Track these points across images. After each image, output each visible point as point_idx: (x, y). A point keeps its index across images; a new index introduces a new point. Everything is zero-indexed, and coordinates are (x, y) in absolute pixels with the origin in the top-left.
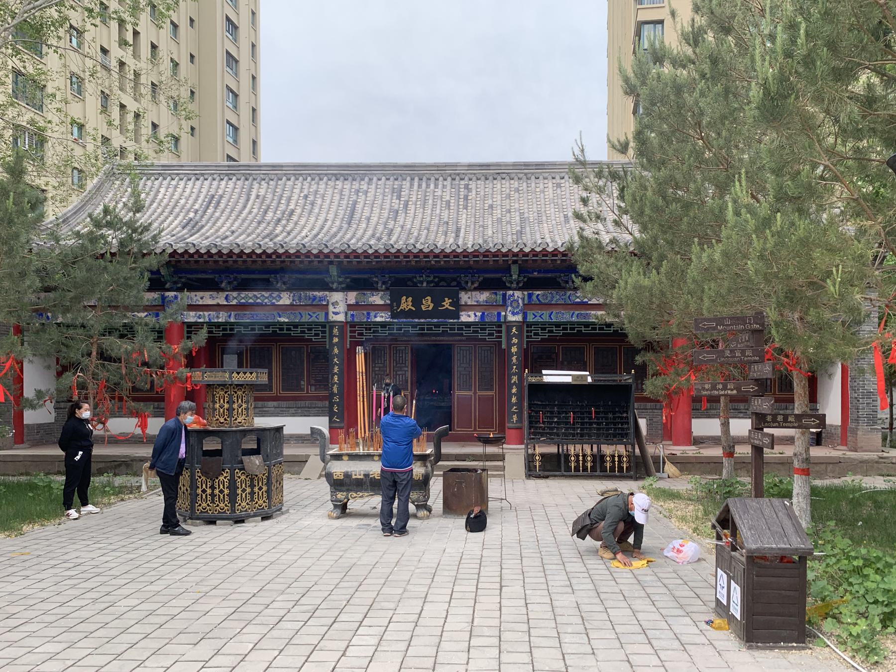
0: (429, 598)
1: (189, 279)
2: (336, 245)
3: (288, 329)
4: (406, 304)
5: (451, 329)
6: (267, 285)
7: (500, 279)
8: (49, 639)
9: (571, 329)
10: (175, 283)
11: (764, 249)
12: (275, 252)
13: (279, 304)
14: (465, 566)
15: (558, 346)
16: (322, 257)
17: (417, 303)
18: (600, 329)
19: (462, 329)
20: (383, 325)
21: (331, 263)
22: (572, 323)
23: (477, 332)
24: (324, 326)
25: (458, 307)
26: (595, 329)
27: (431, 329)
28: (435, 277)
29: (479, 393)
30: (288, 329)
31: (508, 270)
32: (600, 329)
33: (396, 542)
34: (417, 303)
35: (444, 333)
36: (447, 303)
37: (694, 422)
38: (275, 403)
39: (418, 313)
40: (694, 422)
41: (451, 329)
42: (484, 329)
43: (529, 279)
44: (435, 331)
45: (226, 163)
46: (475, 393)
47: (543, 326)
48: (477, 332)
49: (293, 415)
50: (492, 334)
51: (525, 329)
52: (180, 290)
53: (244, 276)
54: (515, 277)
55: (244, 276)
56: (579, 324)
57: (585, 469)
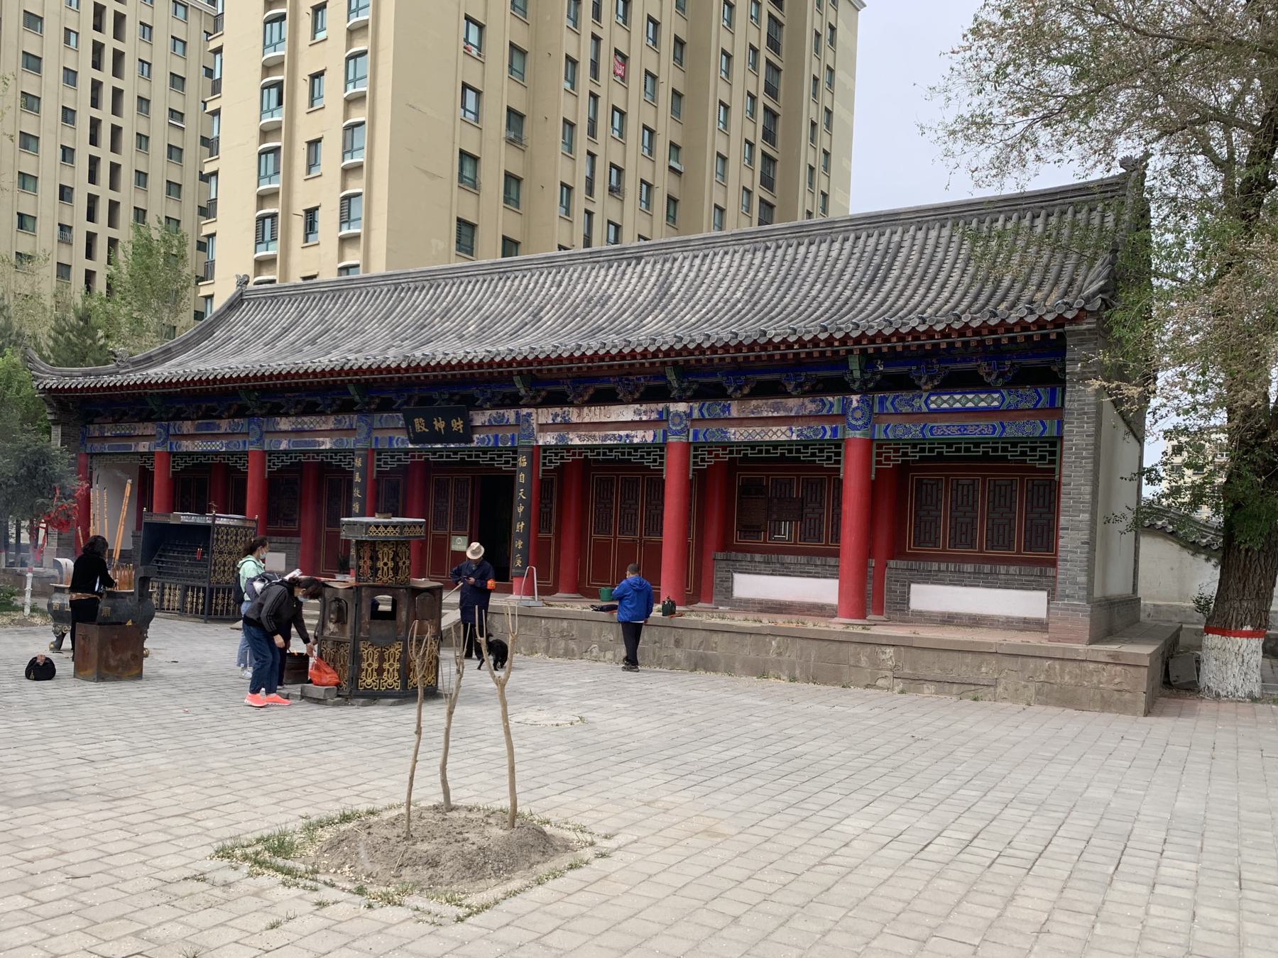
1: (701, 384)
2: (847, 324)
6: (607, 398)
7: (778, 382)
9: (931, 450)
10: (684, 390)
12: (784, 341)
13: (287, 435)
14: (1026, 854)
15: (768, 476)
16: (969, 333)
17: (429, 424)
18: (967, 450)
19: (1005, 449)
20: (286, 452)
21: (850, 352)
25: (470, 429)
29: (620, 537)
30: (477, 456)
31: (843, 363)
32: (967, 450)
38: (283, 539)
41: (470, 456)
43: (549, 392)
45: (636, 244)
47: (898, 445)
49: (1007, 586)
51: (692, 453)
52: (537, 406)
53: (759, 377)
54: (857, 374)
55: (759, 377)
56: (586, 447)
57: (197, 612)
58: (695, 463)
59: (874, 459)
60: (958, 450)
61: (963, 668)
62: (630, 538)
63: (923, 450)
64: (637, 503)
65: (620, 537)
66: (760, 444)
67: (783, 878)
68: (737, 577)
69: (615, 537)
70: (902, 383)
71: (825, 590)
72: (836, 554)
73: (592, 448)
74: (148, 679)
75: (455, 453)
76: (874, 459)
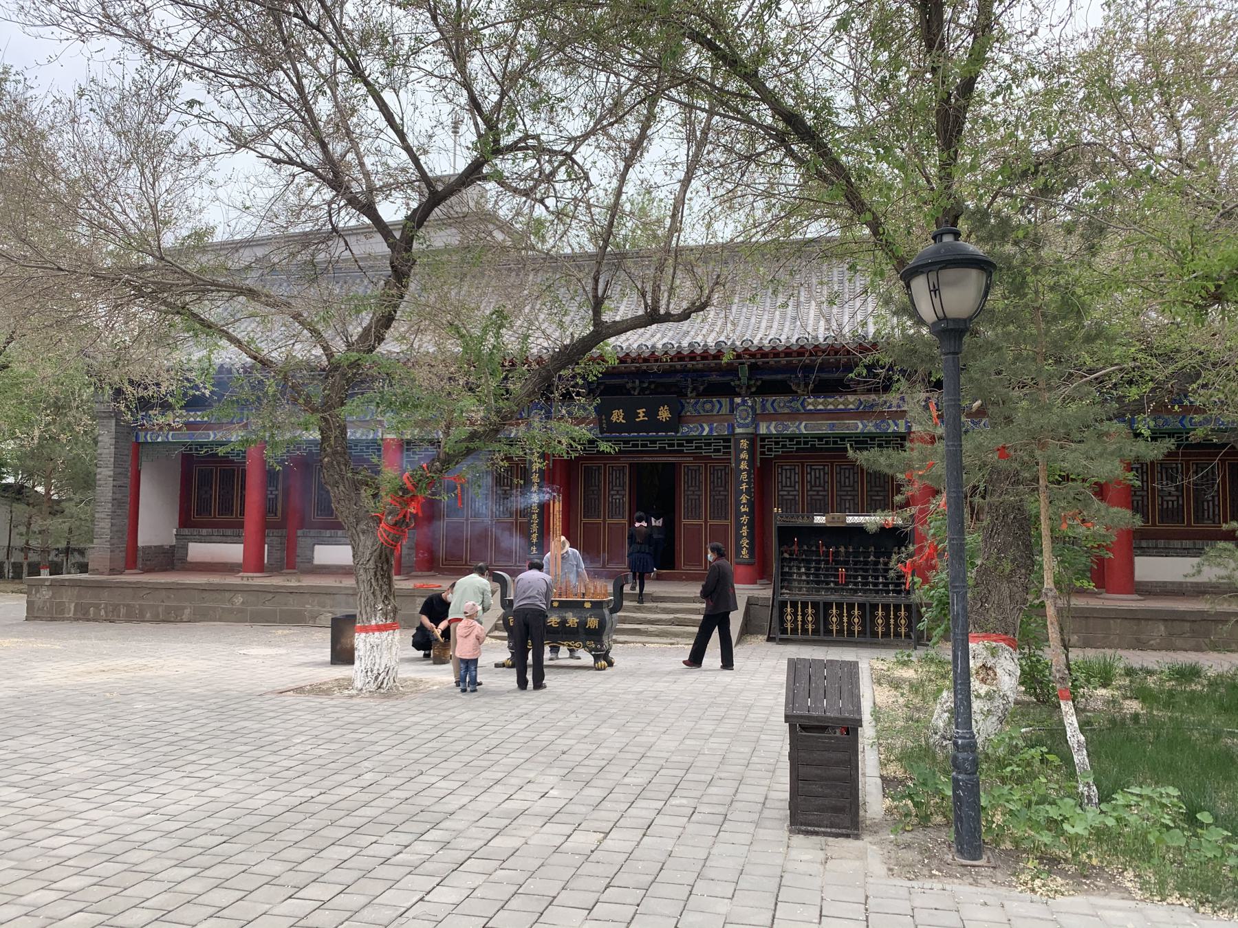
0: (721, 818)
3: (679, 445)
4: (618, 416)
5: (670, 445)
7: (783, 382)
8: (147, 876)
11: (1110, 340)
17: (630, 415)
19: (682, 445)
22: (805, 436)
23: (700, 448)
24: (728, 441)
26: (827, 443)
27: (646, 446)
28: (650, 383)
29: (710, 522)
33: (531, 698)
34: (652, 413)
35: (662, 451)
36: (664, 414)
37: (1138, 560)
39: (631, 425)
40: (1138, 560)
41: (670, 445)
42: (710, 444)
43: (764, 382)
44: (651, 447)
46: (706, 522)
48: (700, 448)
50: (719, 451)
56: (814, 437)
58: (762, 453)
59: (759, 450)
60: (827, 443)
61: (293, 604)
62: (723, 522)
63: (798, 443)
64: (700, 490)
65: (710, 522)
66: (827, 436)
67: (627, 780)
68: (191, 545)
69: (706, 522)
70: (782, 388)
71: (233, 552)
72: (241, 525)
73: (820, 438)
74: (488, 693)
75: (653, 442)
76: (759, 450)
